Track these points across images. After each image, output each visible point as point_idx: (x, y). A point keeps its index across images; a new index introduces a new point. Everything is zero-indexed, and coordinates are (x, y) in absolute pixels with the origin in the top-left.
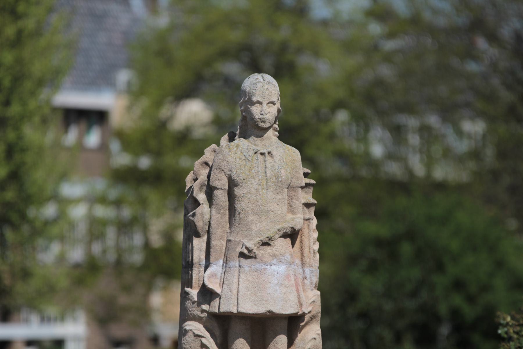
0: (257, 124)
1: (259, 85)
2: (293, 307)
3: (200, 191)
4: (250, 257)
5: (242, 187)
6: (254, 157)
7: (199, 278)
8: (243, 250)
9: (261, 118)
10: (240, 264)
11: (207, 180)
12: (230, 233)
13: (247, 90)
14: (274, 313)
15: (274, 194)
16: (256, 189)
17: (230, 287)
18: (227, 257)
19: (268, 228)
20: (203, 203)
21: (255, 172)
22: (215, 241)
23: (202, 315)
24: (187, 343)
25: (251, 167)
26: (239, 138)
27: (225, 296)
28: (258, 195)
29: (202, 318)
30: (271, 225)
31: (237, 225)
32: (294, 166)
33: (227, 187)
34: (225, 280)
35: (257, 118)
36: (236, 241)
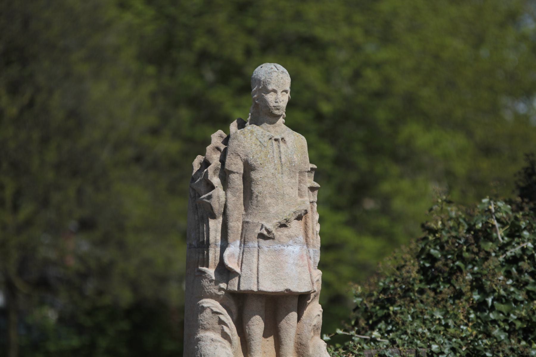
0: (272, 112)
1: (275, 74)
2: (307, 286)
3: (214, 175)
4: (268, 238)
5: (259, 171)
6: (269, 143)
7: (215, 258)
8: (263, 231)
9: (276, 106)
10: (260, 245)
11: (221, 164)
12: (247, 215)
13: (262, 79)
14: (291, 291)
15: (289, 178)
16: (273, 174)
17: (250, 267)
18: (244, 238)
19: (285, 210)
20: (217, 186)
21: (271, 157)
22: (232, 222)
23: (219, 293)
24: (204, 319)
25: (267, 152)
26: (250, 124)
27: (245, 275)
28: (275, 179)
29: (219, 296)
30: (287, 208)
31: (255, 207)
32: (303, 152)
33: (242, 171)
34: (244, 260)
35: (272, 105)
36: (255, 223)
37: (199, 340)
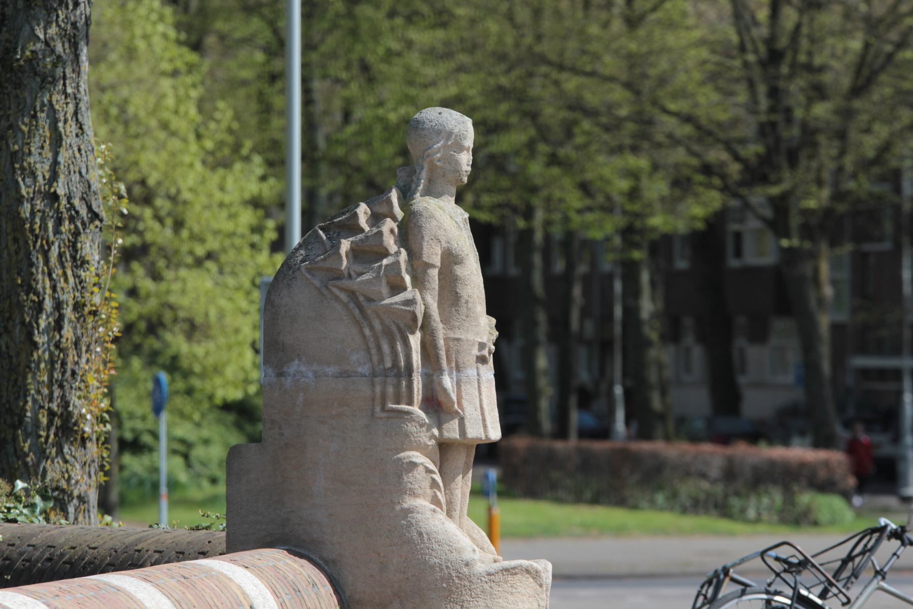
0: (461, 179)
35: (464, 170)
36: (470, 341)
37: (408, 511)
